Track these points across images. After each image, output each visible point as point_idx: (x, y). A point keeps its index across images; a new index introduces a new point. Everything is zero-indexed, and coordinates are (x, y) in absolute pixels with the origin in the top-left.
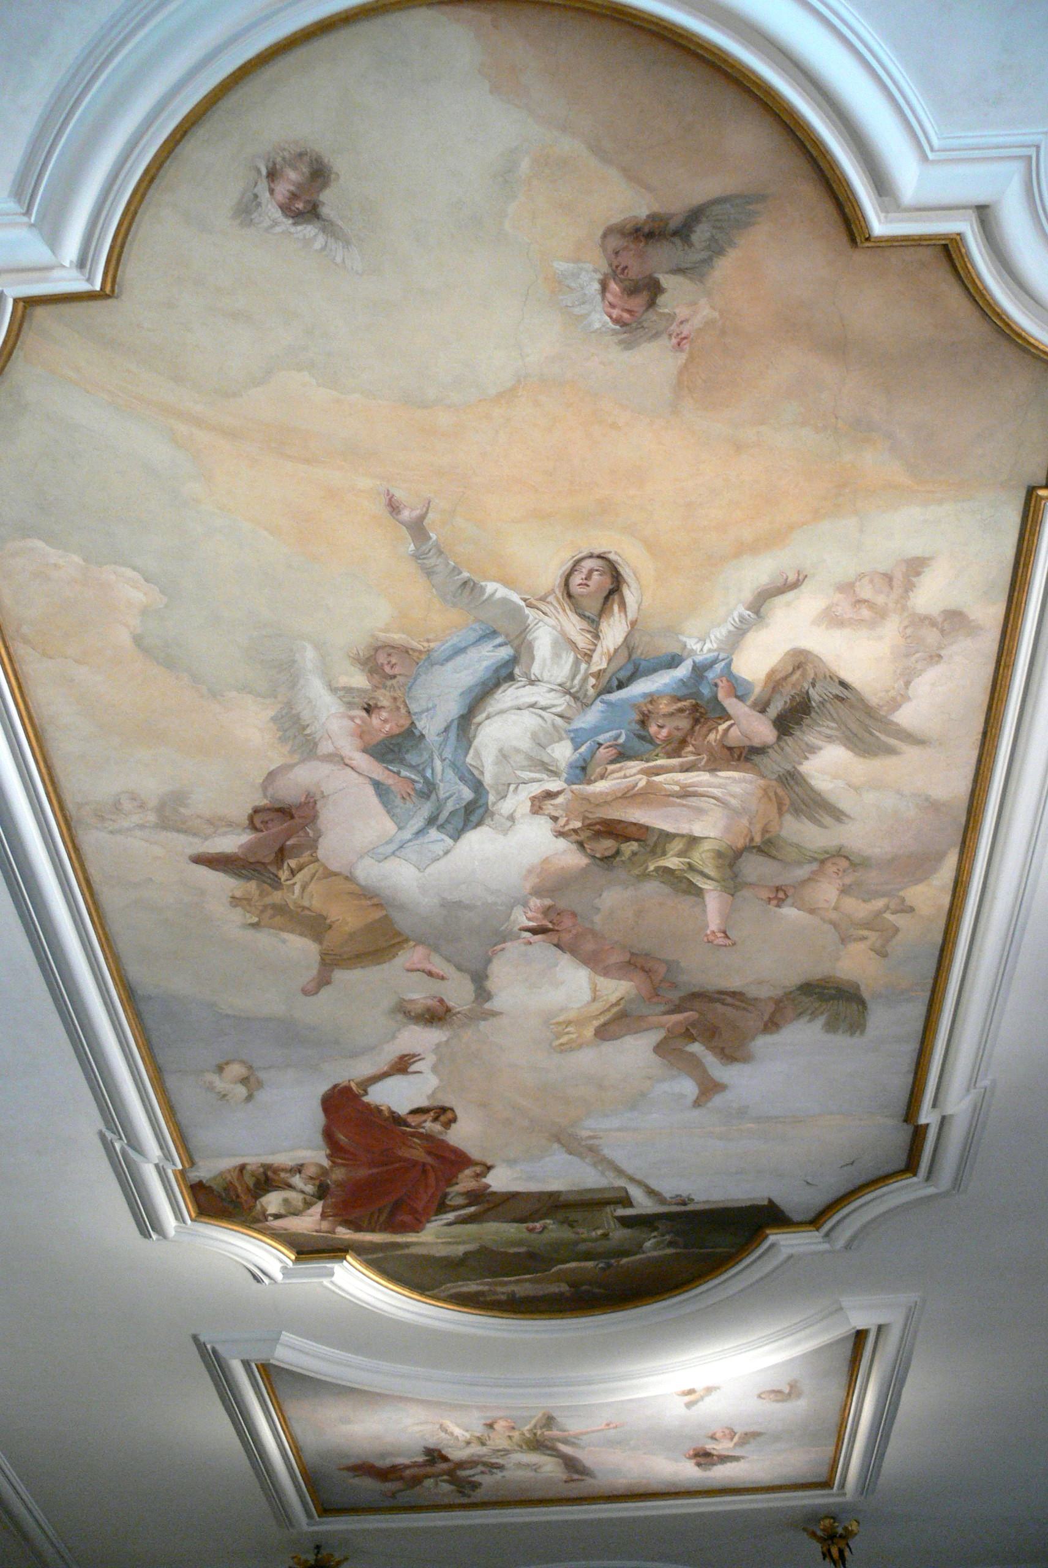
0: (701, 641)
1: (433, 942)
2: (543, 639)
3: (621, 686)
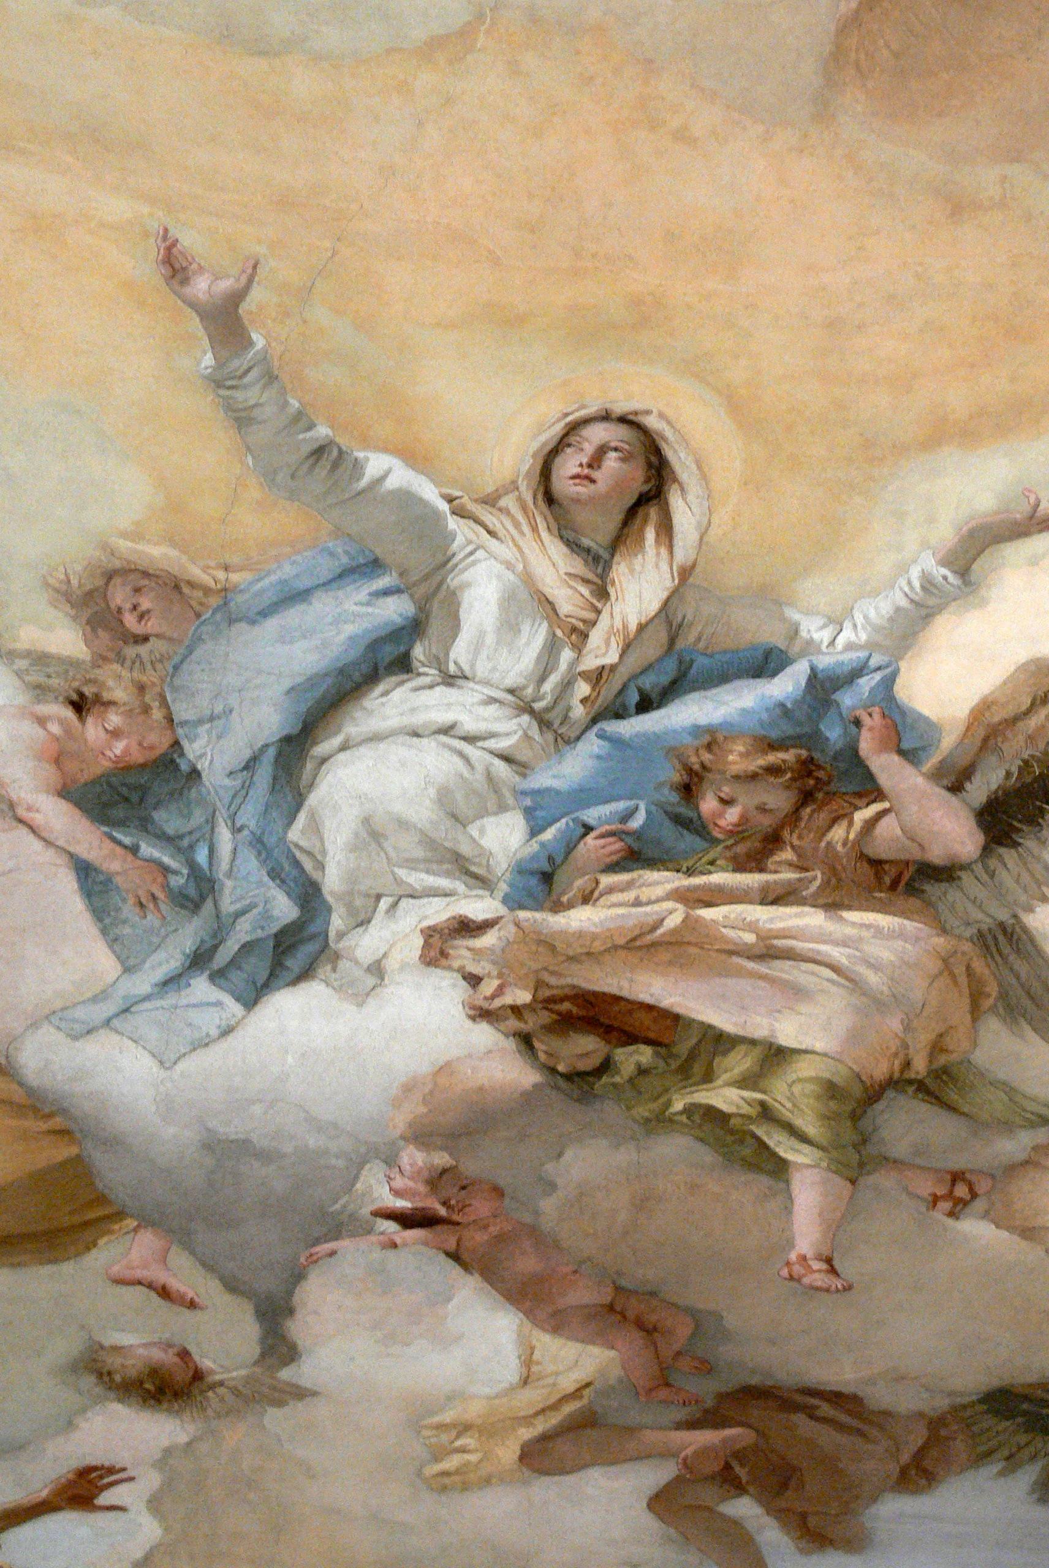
0: (833, 623)
2: (482, 589)
3: (645, 705)
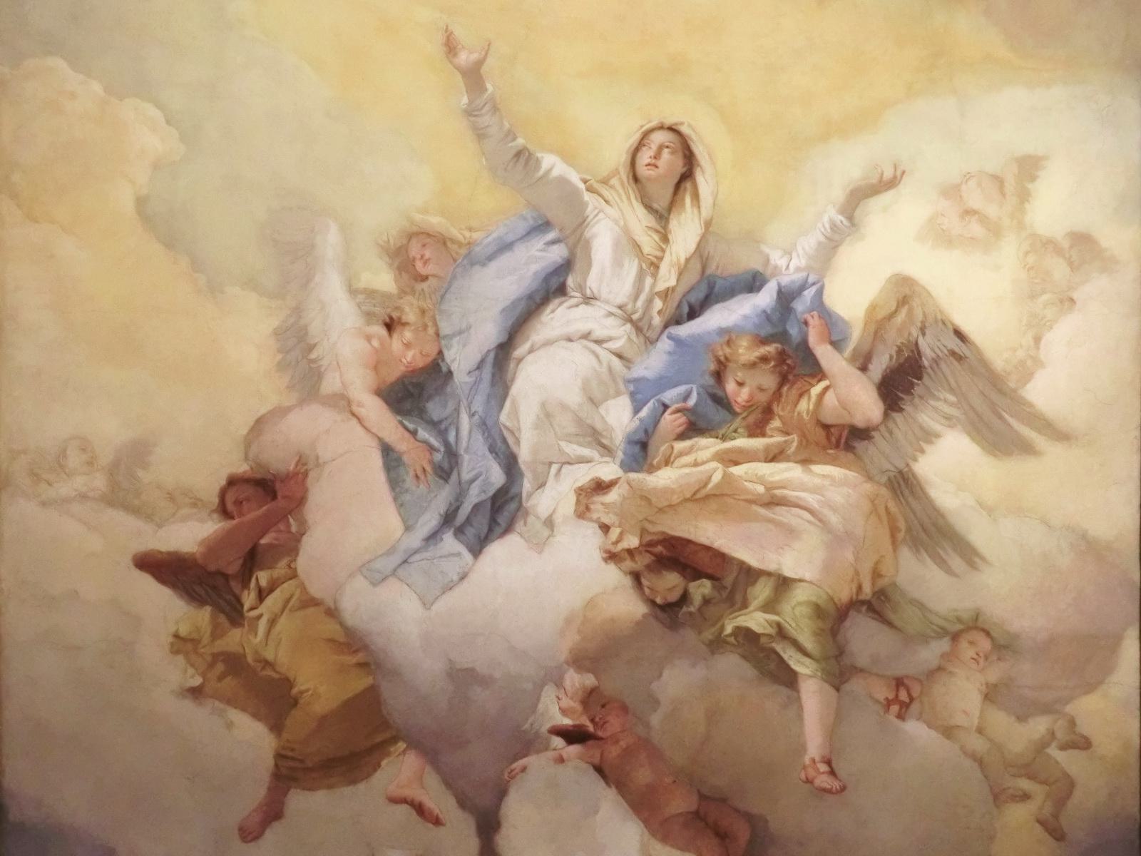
1: (431, 749)
